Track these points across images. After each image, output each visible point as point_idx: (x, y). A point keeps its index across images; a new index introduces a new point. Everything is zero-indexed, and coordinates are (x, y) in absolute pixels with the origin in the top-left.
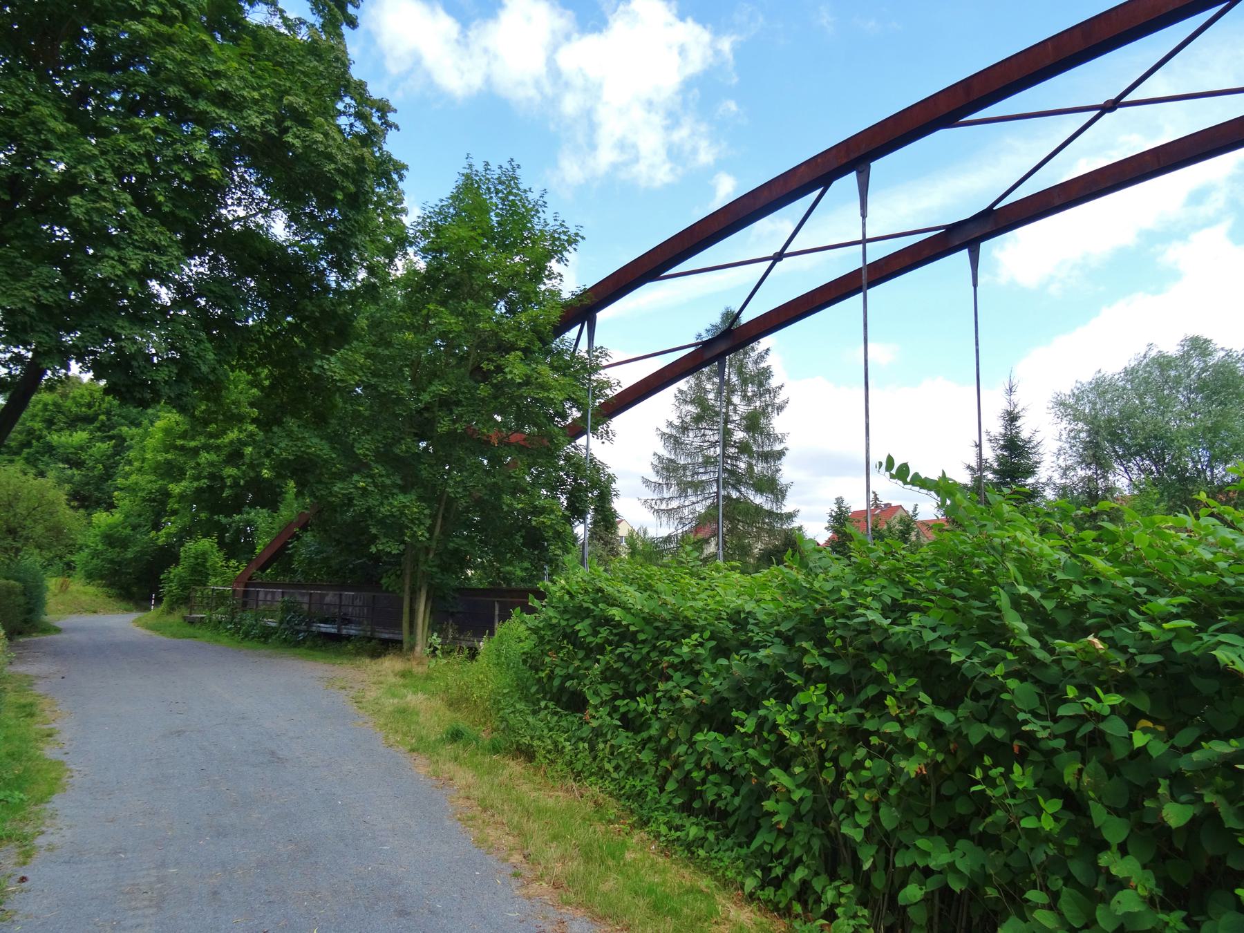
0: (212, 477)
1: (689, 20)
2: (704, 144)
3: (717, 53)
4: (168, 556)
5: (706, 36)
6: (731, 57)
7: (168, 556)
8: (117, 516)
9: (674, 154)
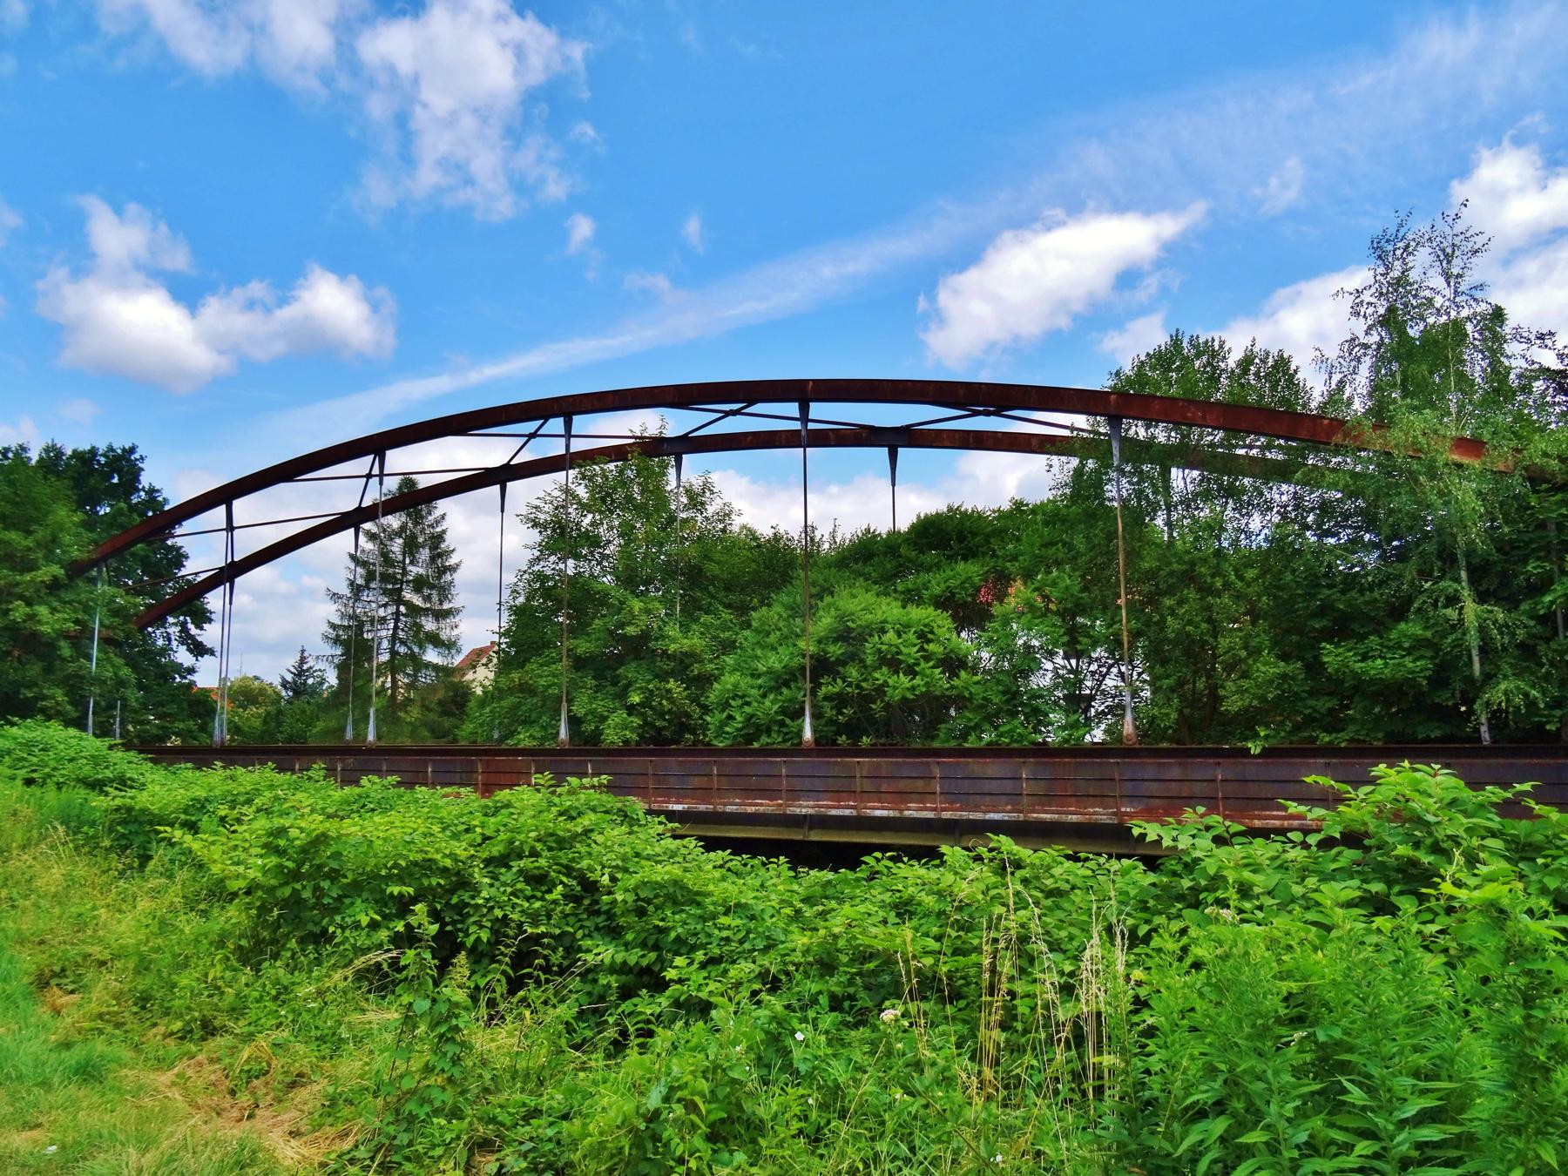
1: (530, 15)
2: (553, 174)
3: (567, 60)
5: (549, 38)
6: (581, 67)
9: (520, 186)
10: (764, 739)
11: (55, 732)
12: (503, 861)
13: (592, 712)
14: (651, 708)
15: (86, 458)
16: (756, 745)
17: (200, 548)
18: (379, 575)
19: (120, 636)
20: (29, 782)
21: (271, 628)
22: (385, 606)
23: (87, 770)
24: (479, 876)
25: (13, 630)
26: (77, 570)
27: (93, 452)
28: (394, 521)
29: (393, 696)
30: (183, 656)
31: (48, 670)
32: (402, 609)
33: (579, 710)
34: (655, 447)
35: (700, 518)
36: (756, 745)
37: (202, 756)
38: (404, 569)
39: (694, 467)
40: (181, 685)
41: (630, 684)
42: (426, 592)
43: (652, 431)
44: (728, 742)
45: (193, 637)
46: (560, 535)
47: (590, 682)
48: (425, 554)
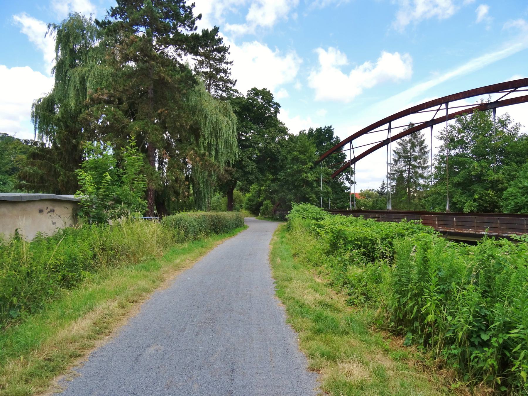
0: (269, 186)
4: (261, 204)
7: (261, 204)
8: (250, 194)
10: (522, 211)
11: (309, 206)
12: (385, 239)
13: (460, 201)
14: (482, 200)
15: (319, 130)
16: (519, 213)
17: (349, 154)
18: (404, 156)
19: (328, 180)
20: (303, 218)
21: (371, 175)
22: (405, 166)
23: (315, 216)
24: (379, 241)
25: (303, 180)
26: (317, 163)
27: (321, 129)
28: (407, 138)
29: (409, 195)
30: (347, 184)
31: (312, 190)
32: (411, 167)
33: (455, 200)
34: (483, 107)
35: (505, 130)
36: (519, 213)
37: (343, 211)
38: (411, 154)
39: (501, 112)
40: (347, 193)
41: (475, 192)
42: (418, 161)
43: (485, 101)
44: (509, 212)
45: (349, 179)
46: (451, 141)
47: (460, 191)
48: (417, 149)
